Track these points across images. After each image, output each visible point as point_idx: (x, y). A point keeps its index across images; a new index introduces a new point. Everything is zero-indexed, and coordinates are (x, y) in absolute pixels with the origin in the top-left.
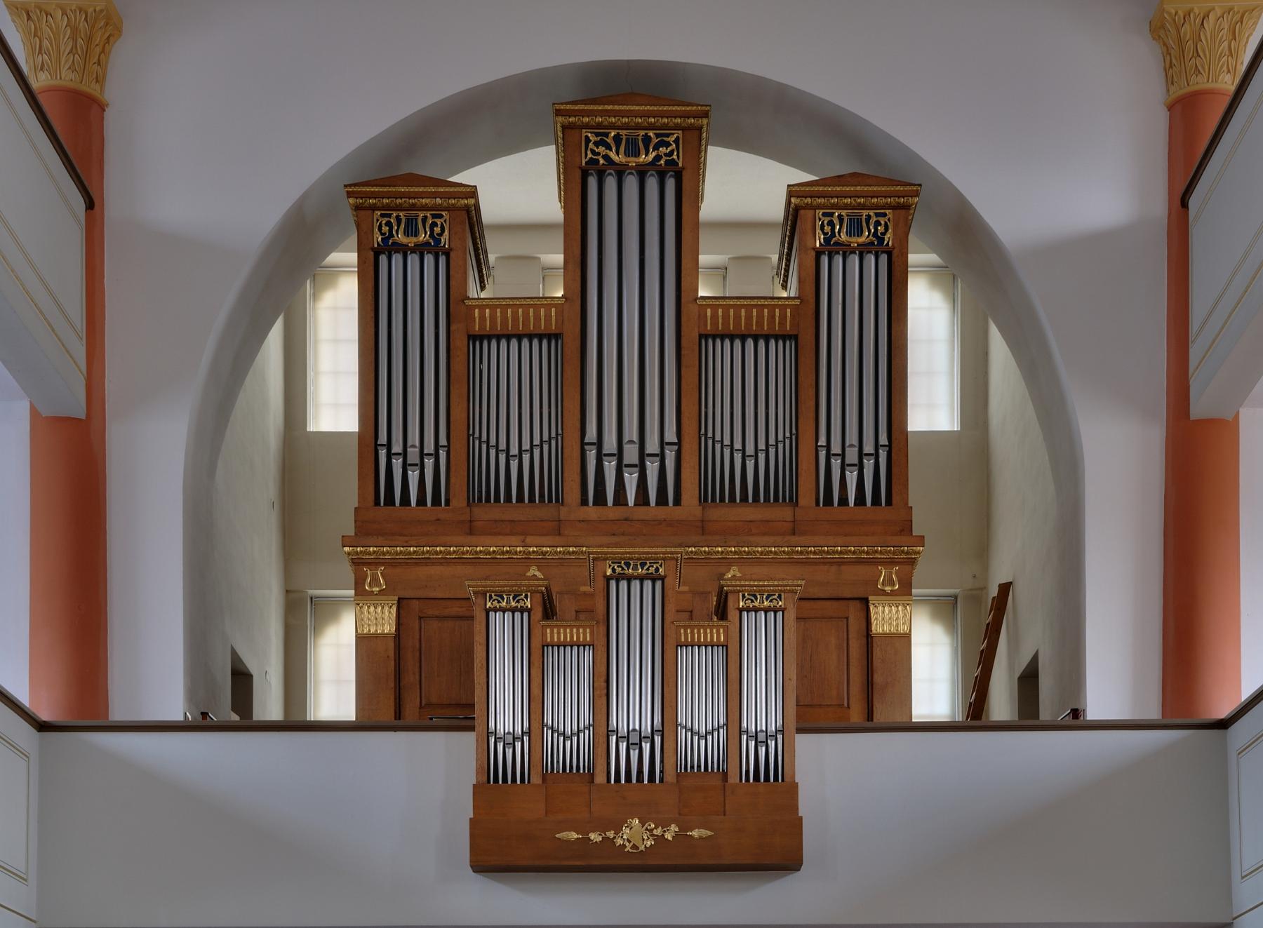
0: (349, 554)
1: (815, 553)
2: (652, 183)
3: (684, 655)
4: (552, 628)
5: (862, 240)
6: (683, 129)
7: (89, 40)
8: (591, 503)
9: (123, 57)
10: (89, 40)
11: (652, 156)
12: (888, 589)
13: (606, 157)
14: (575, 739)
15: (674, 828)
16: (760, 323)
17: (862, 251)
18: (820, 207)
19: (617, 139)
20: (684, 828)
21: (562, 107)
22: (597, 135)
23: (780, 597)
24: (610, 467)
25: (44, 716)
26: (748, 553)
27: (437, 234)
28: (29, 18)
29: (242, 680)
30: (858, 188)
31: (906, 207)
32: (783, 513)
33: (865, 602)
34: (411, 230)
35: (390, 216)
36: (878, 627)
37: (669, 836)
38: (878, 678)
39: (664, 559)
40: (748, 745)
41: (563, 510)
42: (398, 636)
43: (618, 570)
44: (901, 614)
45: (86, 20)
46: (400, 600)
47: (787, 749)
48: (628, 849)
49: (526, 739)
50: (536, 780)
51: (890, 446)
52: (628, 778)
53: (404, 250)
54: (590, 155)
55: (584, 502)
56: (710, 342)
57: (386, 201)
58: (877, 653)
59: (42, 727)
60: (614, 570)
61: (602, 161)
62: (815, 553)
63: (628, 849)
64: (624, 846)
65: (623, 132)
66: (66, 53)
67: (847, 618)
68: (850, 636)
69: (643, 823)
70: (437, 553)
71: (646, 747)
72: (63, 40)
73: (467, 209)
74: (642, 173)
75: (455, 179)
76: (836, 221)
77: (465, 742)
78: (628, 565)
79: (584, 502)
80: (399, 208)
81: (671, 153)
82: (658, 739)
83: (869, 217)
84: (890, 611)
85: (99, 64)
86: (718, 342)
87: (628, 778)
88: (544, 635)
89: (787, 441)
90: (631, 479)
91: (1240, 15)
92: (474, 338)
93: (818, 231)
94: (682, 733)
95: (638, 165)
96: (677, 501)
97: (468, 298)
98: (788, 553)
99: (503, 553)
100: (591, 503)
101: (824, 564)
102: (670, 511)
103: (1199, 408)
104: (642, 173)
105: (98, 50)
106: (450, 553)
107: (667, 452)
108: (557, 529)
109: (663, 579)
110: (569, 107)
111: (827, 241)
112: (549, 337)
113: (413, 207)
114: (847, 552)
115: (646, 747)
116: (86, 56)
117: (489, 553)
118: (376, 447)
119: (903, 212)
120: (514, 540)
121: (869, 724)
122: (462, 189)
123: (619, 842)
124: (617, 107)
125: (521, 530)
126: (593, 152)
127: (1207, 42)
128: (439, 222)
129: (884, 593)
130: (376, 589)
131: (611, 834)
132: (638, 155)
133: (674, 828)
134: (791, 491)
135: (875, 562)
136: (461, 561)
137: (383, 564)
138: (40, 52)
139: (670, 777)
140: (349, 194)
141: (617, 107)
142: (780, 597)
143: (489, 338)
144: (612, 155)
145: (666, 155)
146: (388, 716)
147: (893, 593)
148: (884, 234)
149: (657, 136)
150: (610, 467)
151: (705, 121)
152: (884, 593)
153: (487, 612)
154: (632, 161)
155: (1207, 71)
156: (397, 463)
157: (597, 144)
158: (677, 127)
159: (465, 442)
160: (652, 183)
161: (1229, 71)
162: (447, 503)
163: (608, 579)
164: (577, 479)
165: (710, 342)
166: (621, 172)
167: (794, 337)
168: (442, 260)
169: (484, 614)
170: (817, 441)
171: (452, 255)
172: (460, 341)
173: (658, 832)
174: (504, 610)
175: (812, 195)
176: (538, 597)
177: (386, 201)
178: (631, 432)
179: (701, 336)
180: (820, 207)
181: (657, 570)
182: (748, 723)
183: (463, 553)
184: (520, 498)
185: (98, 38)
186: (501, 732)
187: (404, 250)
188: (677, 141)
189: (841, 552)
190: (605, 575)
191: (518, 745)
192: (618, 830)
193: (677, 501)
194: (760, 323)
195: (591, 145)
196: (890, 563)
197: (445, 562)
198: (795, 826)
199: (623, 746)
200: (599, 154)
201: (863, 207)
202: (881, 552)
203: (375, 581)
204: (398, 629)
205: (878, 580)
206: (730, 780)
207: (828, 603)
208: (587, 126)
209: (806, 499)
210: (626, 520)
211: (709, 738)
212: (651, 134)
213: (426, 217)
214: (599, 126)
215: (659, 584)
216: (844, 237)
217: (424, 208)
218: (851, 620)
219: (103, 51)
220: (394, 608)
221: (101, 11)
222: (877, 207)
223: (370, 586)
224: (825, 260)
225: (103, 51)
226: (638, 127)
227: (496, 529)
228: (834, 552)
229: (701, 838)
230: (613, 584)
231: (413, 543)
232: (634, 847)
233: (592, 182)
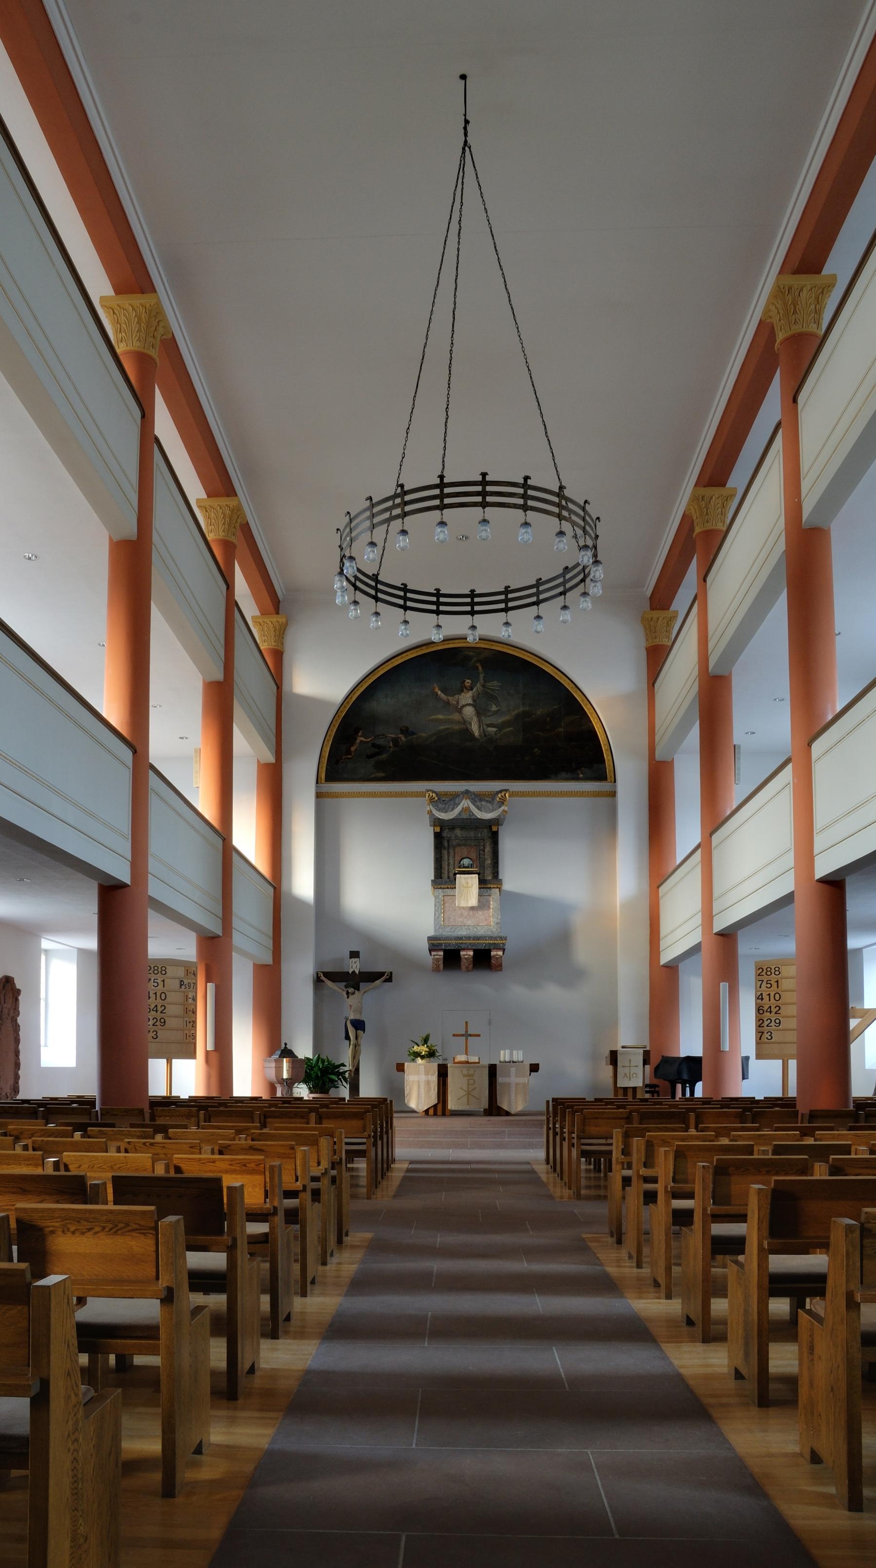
27: (481, 537)
45: (146, 312)
66: (136, 331)
68: (218, 430)
85: (154, 337)
91: (821, 290)
103: (659, 756)
127: (802, 305)
138: (120, 332)
155: (802, 322)
161: (815, 322)
221: (154, 305)
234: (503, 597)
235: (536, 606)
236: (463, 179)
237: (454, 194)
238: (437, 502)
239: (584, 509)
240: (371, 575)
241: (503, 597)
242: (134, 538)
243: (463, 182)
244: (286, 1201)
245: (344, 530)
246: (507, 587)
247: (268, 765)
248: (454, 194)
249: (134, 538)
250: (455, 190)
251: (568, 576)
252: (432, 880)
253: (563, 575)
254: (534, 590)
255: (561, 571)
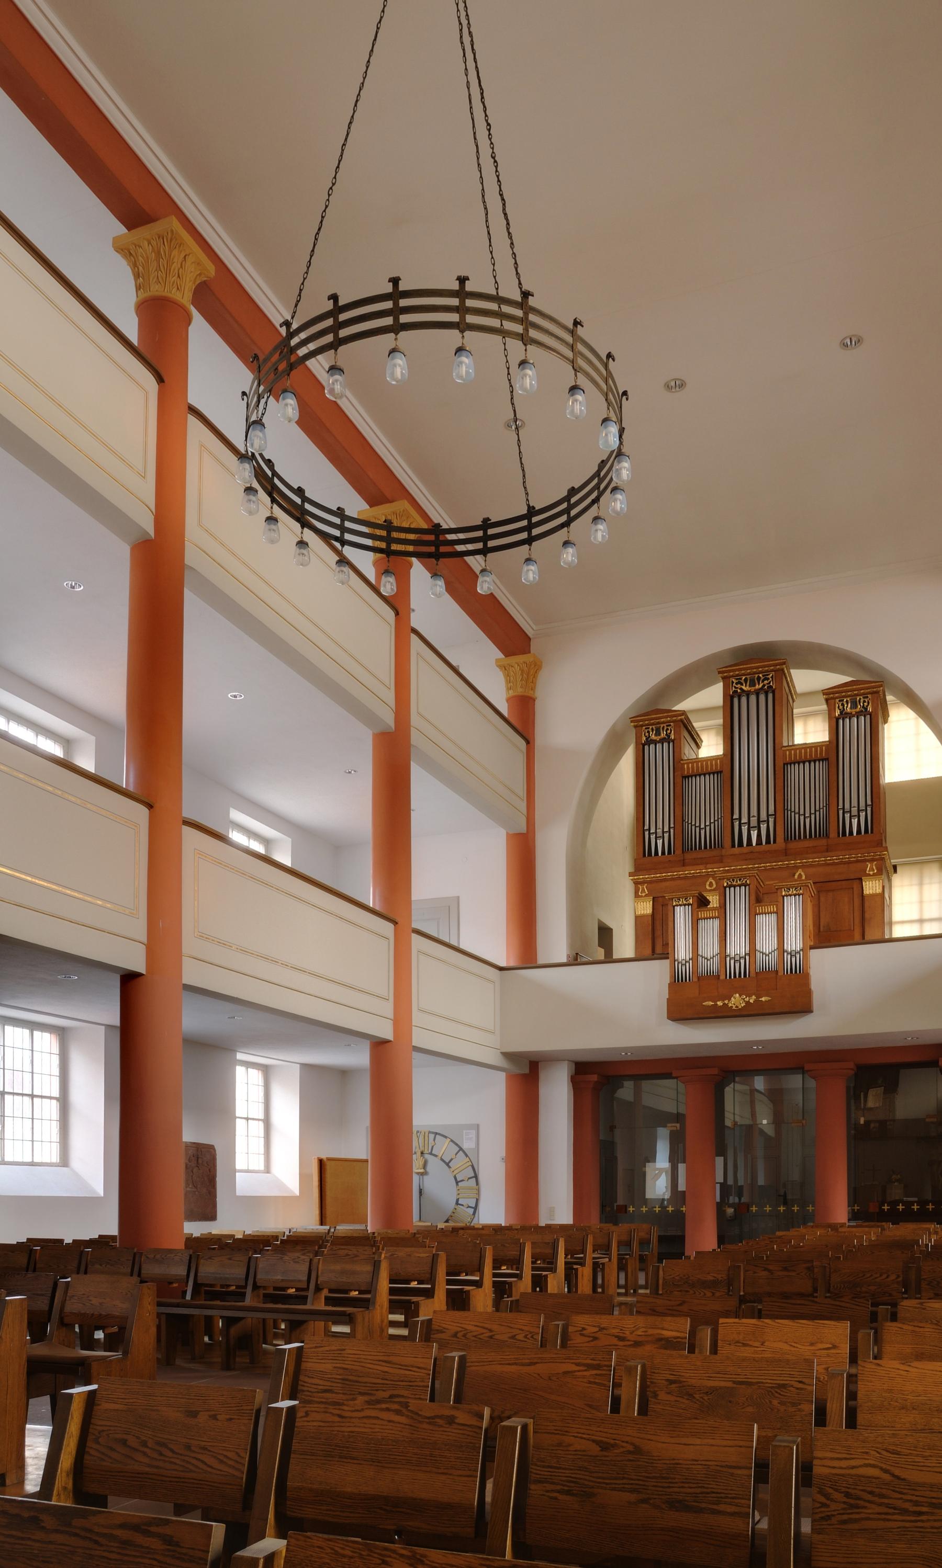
0: (632, 880)
1: (836, 859)
2: (762, 697)
3: (758, 918)
4: (701, 911)
5: (858, 710)
6: (775, 671)
7: (528, 674)
8: (736, 846)
9: (543, 676)
10: (528, 674)
11: (761, 686)
12: (871, 873)
13: (741, 689)
14: (712, 960)
15: (754, 997)
16: (811, 755)
17: (858, 715)
18: (837, 698)
19: (746, 680)
20: (758, 996)
21: (721, 670)
22: (737, 679)
23: (801, 889)
24: (745, 829)
25: (503, 964)
26: (806, 862)
28: (505, 669)
29: (605, 934)
30: (854, 687)
31: (877, 692)
32: (823, 842)
33: (861, 880)
34: (658, 733)
35: (649, 728)
36: (867, 891)
37: (752, 1001)
38: (867, 916)
39: (749, 876)
40: (787, 957)
41: (724, 851)
42: (653, 915)
43: (730, 883)
44: (877, 885)
46: (653, 898)
47: (806, 958)
48: (734, 1008)
49: (691, 961)
50: (695, 979)
51: (872, 805)
52: (682, 981)
53: (655, 742)
54: (734, 689)
55: (733, 846)
56: (789, 766)
57: (646, 722)
58: (867, 904)
59: (501, 969)
60: (727, 883)
61: (739, 691)
62: (836, 859)
63: (734, 1008)
64: (732, 1007)
65: (748, 677)
67: (853, 888)
69: (740, 996)
70: (669, 876)
71: (742, 961)
72: (194, 1458)
73: (681, 721)
74: (757, 693)
75: (674, 709)
76: (845, 703)
77: (666, 963)
78: (733, 880)
79: (733, 846)
80: (653, 724)
81: (770, 682)
82: (747, 958)
83: (860, 699)
84: (872, 883)
86: (793, 765)
87: (682, 981)
88: (698, 915)
89: (825, 808)
90: (754, 834)
92: (684, 777)
93: (837, 709)
94: (758, 954)
95: (755, 690)
96: (775, 842)
97: (682, 760)
98: (824, 861)
99: (697, 873)
100: (736, 846)
101: (841, 864)
102: (772, 846)
104: (757, 693)
105: (532, 677)
106: (674, 875)
107: (770, 819)
108: (721, 860)
109: (749, 885)
110: (724, 669)
111: (841, 713)
112: (717, 773)
113: (659, 723)
114: (851, 858)
115: (742, 961)
116: (527, 681)
117: (691, 874)
118: (644, 831)
119: (876, 695)
120: (701, 867)
121: (864, 941)
122: (679, 713)
123: (730, 1005)
124: (745, 666)
125: (705, 862)
126: (735, 687)
128: (669, 728)
129: (869, 875)
130: (644, 894)
131: (726, 1002)
132: (755, 685)
133: (754, 997)
134: (826, 830)
135: (865, 861)
136: (679, 878)
137: (646, 883)
139: (753, 974)
140: (632, 722)
141: (745, 666)
142: (801, 889)
143: (688, 777)
144: (744, 687)
145: (767, 684)
146: (648, 951)
147: (874, 875)
148: (867, 706)
149: (763, 676)
150: (745, 829)
151: (784, 666)
152: (869, 875)
153: (674, 907)
154: (753, 689)
156: (653, 837)
157: (737, 684)
158: (772, 671)
159: (681, 825)
160: (762, 697)
162: (674, 853)
163: (725, 888)
164: (730, 835)
165: (789, 766)
166: (748, 694)
167: (827, 759)
168: (671, 744)
169: (672, 908)
170: (838, 806)
171: (675, 742)
172: (679, 780)
173: (747, 999)
174: (681, 905)
175: (833, 693)
176: (695, 898)
177: (646, 722)
178: (754, 812)
179: (784, 764)
180: (837, 698)
181: (746, 881)
182: (788, 947)
183: (680, 875)
184: (705, 847)
185: (532, 672)
186: (680, 959)
187: (655, 742)
188: (772, 677)
189: (848, 858)
190: (724, 886)
191: (687, 964)
192: (729, 1000)
193: (775, 842)
194: (811, 755)
195: (734, 684)
196: (872, 861)
197: (673, 879)
198: (808, 993)
199: (732, 962)
200: (737, 688)
201: (857, 695)
202: (867, 856)
203: (643, 891)
204: (653, 912)
205: (866, 870)
206: (779, 974)
207: (844, 882)
208: (732, 676)
209: (833, 834)
210: (751, 852)
211: (770, 955)
212: (761, 675)
213: (664, 727)
214: (738, 675)
215: (747, 887)
216: (849, 710)
217: (663, 723)
218: (855, 889)
219: (534, 677)
220: (651, 902)
222: (864, 694)
223: (641, 893)
224: (841, 721)
225: (534, 677)
226: (755, 673)
227: (695, 863)
228: (845, 858)
229: (766, 1001)
230: (728, 889)
231: (659, 872)
232: (737, 1007)
233: (736, 700)
234: (480, 533)
235: (527, 546)
236: (469, 29)
237: (462, 43)
238: (388, 321)
239: (606, 366)
240: (335, 509)
241: (480, 533)
242: (525, 832)
243: (470, 33)
244: (272, 1321)
245: (265, 360)
246: (486, 520)
247: (520, 835)
248: (462, 43)
249: (525, 832)
250: (461, 37)
251: (573, 500)
252: (192, 1234)
253: (567, 498)
254: (524, 523)
255: (565, 494)
